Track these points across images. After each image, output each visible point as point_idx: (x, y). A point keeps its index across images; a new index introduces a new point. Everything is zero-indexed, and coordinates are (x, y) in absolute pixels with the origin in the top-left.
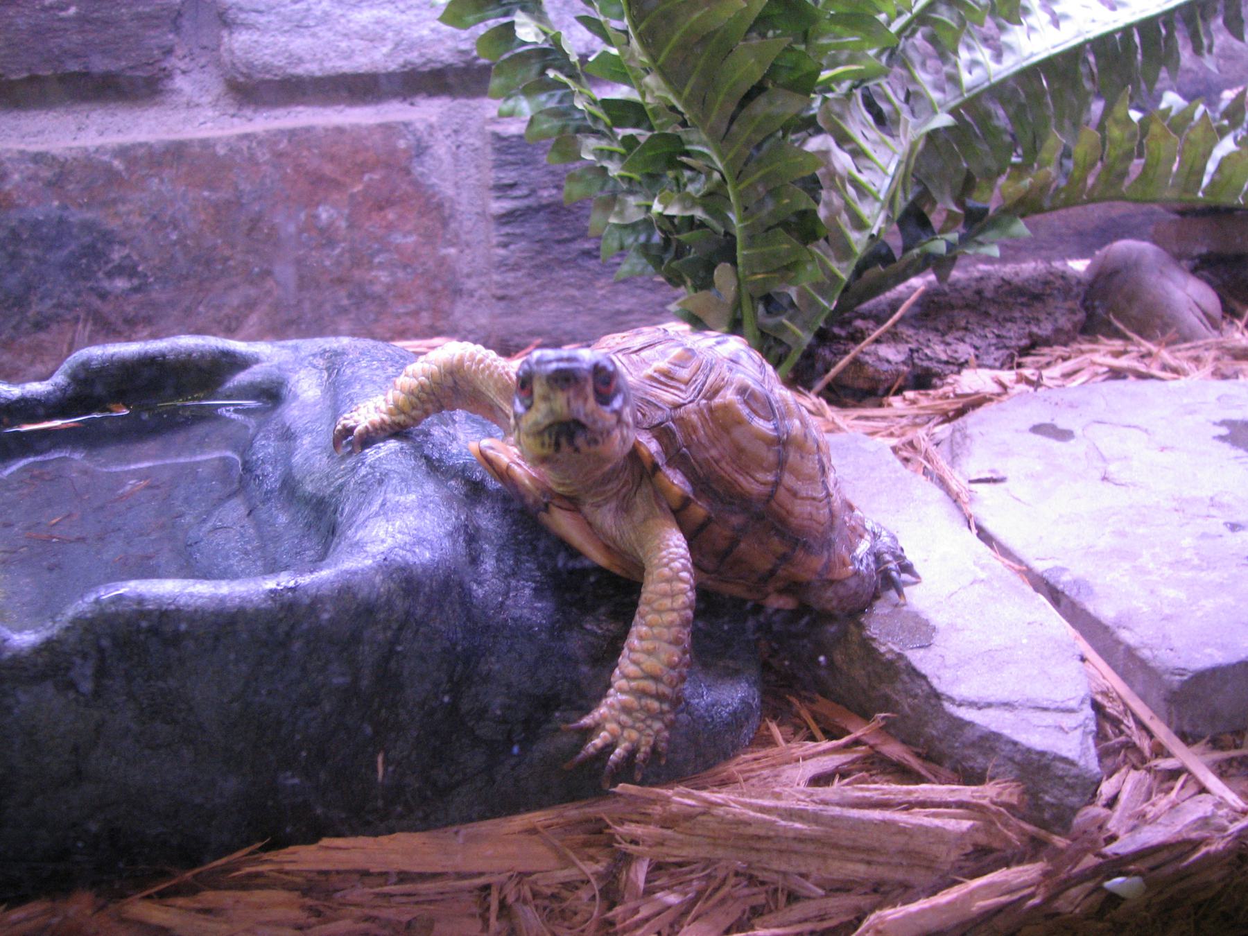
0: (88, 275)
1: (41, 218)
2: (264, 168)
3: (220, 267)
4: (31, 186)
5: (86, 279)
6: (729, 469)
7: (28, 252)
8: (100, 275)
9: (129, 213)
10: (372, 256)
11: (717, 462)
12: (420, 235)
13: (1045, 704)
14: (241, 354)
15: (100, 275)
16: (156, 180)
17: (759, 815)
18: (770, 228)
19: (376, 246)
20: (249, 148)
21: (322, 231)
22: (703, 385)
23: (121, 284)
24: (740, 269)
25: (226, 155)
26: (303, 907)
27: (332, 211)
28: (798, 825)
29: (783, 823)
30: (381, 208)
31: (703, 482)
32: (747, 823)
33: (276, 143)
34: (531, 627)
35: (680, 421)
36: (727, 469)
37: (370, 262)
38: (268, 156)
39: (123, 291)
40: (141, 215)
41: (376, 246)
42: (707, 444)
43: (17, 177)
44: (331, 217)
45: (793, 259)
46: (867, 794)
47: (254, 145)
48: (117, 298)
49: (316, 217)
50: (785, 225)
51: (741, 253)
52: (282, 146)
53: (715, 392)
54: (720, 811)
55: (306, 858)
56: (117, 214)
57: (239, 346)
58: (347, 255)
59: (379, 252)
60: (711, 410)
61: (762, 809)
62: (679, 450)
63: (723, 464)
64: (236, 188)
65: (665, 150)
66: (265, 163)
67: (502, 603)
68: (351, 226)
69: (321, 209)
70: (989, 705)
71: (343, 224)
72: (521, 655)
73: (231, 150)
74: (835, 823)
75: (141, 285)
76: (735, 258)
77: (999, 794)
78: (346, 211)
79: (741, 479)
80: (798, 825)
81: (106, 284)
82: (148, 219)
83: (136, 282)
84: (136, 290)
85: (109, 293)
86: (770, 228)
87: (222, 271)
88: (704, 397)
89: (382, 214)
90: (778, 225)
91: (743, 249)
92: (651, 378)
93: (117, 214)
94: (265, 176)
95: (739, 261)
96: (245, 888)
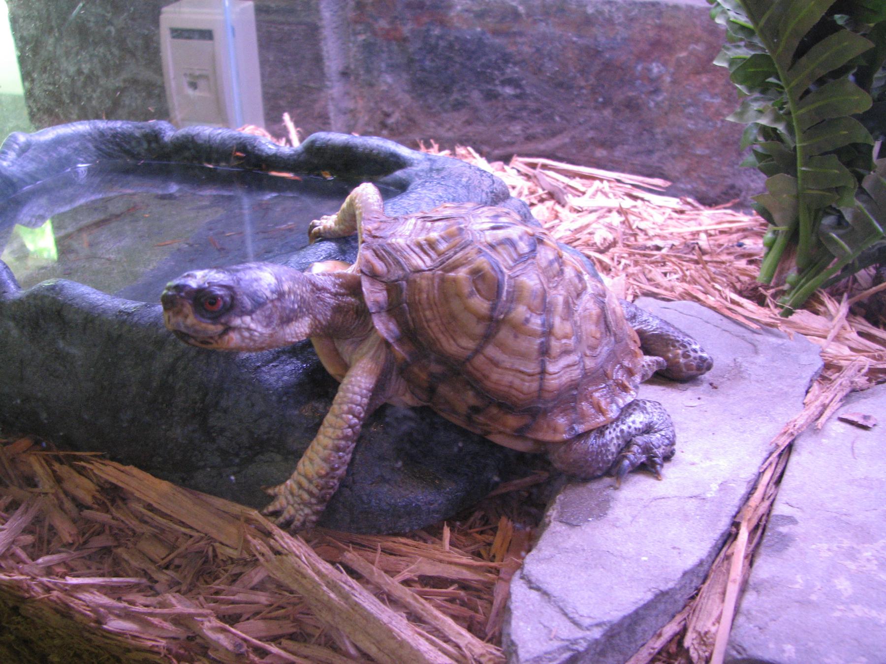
0: (490, 80)
1: (468, 37)
2: (618, 27)
3: (575, 93)
4: (466, 15)
5: (488, 83)
6: (436, 330)
7: (458, 59)
8: (497, 82)
9: (523, 43)
10: (685, 107)
11: (427, 321)
12: (724, 99)
13: (569, 610)
14: (403, 157)
15: (497, 82)
16: (544, 24)
17: (313, 574)
18: (826, 153)
19: (689, 100)
20: (610, 11)
21: (651, 81)
22: (448, 259)
23: (509, 91)
24: (800, 182)
25: (593, 14)
26: (94, 497)
27: (662, 68)
28: (332, 595)
29: (325, 588)
30: (698, 73)
31: (411, 334)
32: (304, 576)
33: (629, 11)
34: (268, 389)
35: (411, 283)
36: (435, 329)
37: (682, 111)
38: (622, 20)
39: (510, 95)
40: (530, 46)
41: (689, 100)
42: (426, 306)
43: (459, 8)
44: (660, 72)
45: (841, 184)
46: (416, 604)
47: (613, 10)
48: (504, 99)
49: (650, 70)
50: (839, 152)
51: (801, 168)
52: (633, 13)
53: (455, 267)
54: (292, 559)
55: (110, 472)
56: (515, 44)
57: (404, 151)
58: (667, 103)
59: (690, 105)
60: (443, 280)
61: (319, 573)
62: (401, 304)
63: (432, 325)
64: (596, 39)
65: (766, 69)
66: (620, 24)
67: (259, 367)
68: (674, 82)
69: (654, 65)
70: (538, 589)
71: (668, 79)
72: (253, 405)
73: (597, 11)
74: (356, 608)
75: (521, 94)
76: (796, 170)
77: (482, 655)
78: (672, 70)
79: (443, 340)
80: (332, 595)
81: (499, 89)
82: (534, 50)
83: (518, 91)
84: (517, 97)
85: (500, 95)
86: (826, 153)
87: (577, 96)
88: (442, 269)
89: (698, 77)
90: (834, 152)
91: (805, 164)
92: (420, 246)
93: (515, 44)
94: (617, 33)
95: (799, 174)
96: (80, 473)
